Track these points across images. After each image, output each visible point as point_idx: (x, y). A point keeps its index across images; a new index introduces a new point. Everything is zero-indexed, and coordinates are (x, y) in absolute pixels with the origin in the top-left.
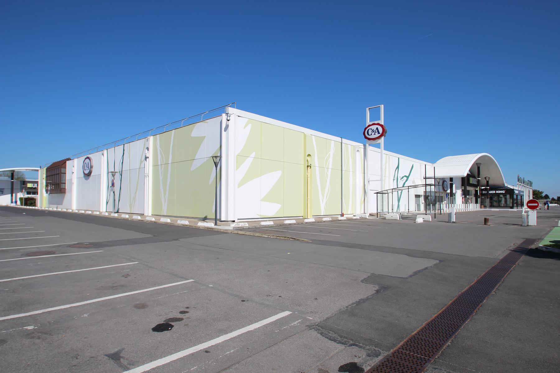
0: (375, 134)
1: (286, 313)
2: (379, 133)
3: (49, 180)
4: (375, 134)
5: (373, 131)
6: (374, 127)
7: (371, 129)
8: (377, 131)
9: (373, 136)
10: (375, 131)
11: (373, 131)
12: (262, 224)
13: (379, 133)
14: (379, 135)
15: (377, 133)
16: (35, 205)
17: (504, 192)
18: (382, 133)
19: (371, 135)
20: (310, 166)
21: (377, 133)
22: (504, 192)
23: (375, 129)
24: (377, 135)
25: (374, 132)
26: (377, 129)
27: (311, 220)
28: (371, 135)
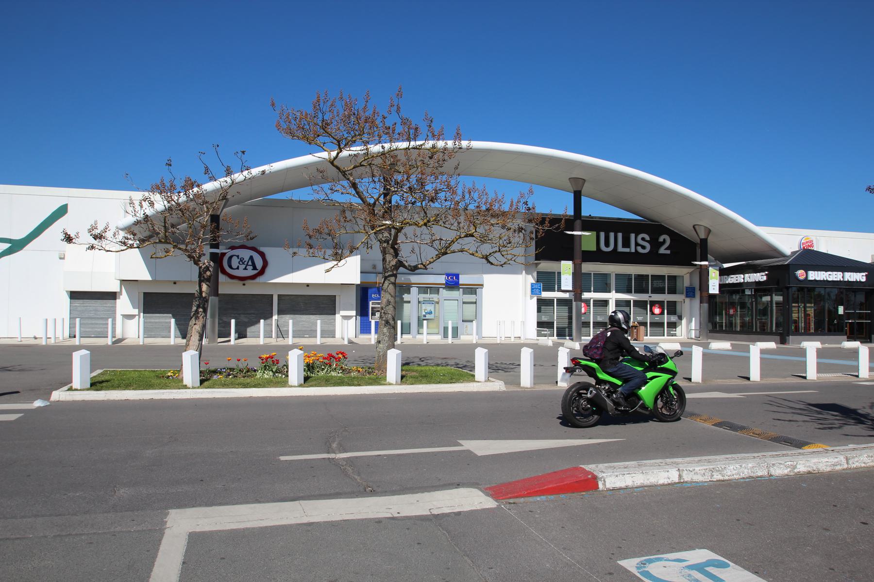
0: (245, 269)
1: (283, 458)
2: (255, 268)
3: (742, 311)
4: (245, 269)
5: (242, 261)
6: (246, 254)
7: (238, 256)
8: (250, 263)
9: (241, 273)
10: (246, 263)
11: (241, 260)
12: (725, 267)
13: (255, 268)
14: (255, 272)
15: (251, 267)
16: (375, 322)
17: (765, 278)
18: (260, 270)
19: (238, 268)
20: (430, 509)
21: (250, 268)
22: (765, 278)
23: (246, 259)
24: (250, 272)
25: (243, 263)
26: (251, 258)
27: (425, 342)
28: (238, 268)
